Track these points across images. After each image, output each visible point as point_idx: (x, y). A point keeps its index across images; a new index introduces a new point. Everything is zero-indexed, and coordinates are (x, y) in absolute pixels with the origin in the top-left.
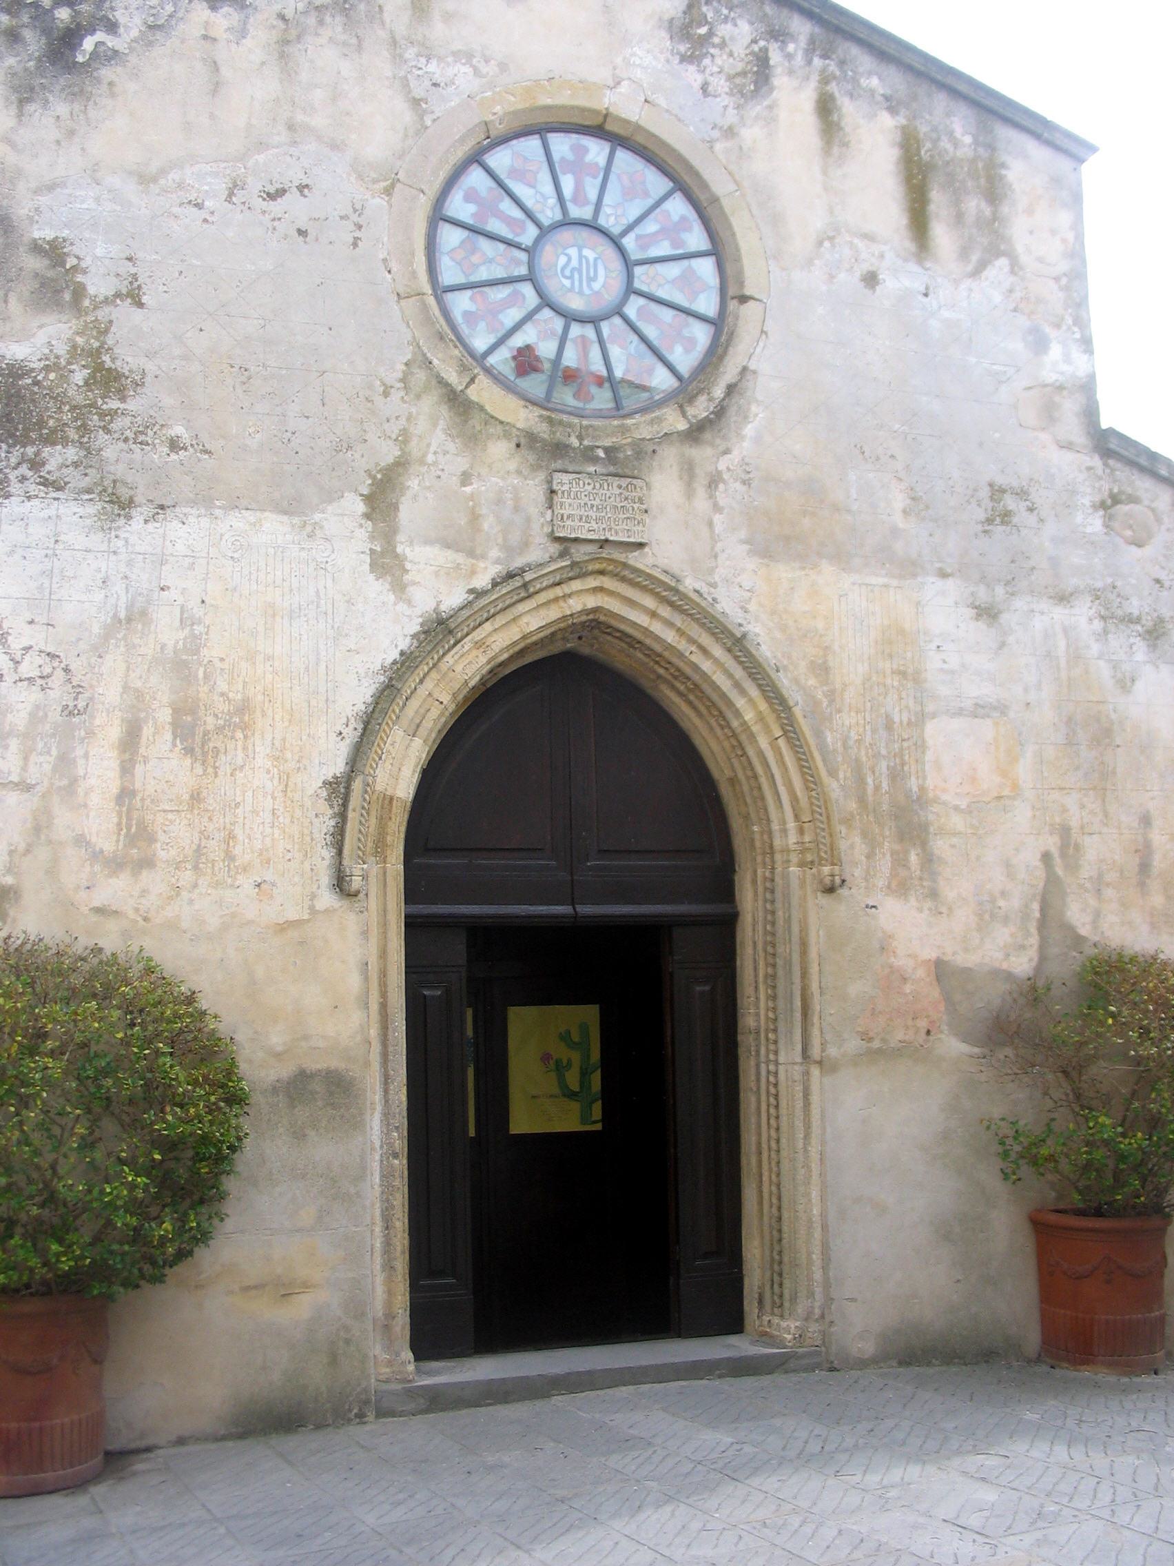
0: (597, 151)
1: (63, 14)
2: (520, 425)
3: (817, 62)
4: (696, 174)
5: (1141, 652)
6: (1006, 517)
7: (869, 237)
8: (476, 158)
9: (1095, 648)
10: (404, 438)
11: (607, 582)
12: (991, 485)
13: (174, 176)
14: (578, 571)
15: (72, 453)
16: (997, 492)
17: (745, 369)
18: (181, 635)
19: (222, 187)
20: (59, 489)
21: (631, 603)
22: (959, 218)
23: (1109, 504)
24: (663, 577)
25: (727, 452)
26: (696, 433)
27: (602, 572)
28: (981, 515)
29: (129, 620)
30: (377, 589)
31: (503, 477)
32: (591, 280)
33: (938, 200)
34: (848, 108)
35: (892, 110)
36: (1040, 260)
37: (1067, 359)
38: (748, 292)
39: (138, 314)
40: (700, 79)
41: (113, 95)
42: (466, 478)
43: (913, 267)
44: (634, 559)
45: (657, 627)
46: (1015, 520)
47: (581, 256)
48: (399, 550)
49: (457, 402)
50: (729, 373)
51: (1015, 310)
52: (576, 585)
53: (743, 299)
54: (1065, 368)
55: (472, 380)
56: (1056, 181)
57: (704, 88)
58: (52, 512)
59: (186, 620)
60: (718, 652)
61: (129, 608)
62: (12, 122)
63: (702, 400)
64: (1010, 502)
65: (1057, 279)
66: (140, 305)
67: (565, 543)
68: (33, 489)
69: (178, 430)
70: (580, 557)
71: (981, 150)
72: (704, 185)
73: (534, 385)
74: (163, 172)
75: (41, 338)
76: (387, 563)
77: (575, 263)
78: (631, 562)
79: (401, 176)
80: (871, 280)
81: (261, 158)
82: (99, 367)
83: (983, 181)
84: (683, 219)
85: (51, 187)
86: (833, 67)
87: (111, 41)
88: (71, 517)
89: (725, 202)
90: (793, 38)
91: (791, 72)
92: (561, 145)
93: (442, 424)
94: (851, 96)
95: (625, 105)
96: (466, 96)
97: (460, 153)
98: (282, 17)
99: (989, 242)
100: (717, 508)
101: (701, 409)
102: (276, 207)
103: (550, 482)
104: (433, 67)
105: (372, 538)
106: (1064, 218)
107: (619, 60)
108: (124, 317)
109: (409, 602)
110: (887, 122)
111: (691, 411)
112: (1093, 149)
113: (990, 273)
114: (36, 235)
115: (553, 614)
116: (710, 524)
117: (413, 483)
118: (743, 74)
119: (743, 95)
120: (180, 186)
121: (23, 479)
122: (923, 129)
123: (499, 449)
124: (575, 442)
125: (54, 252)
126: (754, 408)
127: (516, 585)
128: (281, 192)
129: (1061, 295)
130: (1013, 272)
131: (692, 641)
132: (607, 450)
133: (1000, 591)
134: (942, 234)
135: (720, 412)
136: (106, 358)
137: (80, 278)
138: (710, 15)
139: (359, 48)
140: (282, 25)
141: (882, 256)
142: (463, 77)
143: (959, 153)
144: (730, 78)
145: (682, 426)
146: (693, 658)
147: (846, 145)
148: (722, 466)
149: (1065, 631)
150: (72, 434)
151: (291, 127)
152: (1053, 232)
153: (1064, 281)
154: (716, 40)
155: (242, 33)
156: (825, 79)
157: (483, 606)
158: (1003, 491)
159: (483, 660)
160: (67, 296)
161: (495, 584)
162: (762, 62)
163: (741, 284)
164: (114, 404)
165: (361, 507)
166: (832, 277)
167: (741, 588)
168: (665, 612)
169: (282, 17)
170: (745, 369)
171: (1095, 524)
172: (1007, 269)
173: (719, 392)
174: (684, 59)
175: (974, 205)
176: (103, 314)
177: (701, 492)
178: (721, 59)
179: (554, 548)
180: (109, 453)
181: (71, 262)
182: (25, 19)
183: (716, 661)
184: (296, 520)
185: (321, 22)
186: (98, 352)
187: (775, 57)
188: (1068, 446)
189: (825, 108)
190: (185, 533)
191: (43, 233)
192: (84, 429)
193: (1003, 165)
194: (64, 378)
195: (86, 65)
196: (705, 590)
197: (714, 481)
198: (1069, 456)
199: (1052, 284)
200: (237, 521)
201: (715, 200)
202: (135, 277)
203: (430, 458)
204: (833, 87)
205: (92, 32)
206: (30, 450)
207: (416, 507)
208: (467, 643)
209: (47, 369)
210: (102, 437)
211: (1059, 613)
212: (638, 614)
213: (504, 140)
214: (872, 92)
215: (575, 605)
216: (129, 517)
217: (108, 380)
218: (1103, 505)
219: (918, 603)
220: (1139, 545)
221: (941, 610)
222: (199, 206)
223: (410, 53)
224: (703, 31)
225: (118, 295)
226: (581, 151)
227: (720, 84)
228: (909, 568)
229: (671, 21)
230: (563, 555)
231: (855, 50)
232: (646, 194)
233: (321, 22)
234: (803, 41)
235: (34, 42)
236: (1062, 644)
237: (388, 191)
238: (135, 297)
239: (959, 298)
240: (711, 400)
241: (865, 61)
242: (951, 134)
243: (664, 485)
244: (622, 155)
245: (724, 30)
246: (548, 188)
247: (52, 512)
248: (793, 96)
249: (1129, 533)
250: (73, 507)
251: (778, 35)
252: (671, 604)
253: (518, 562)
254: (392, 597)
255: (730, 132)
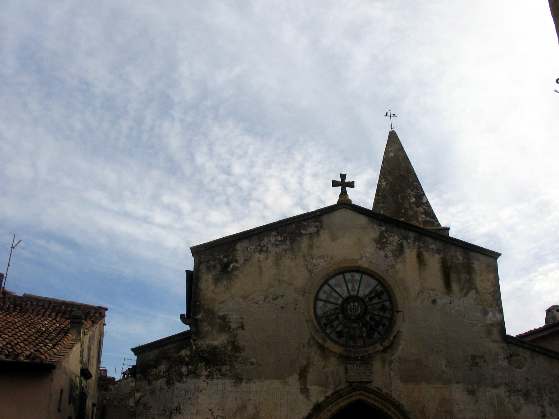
0: (357, 276)
1: (225, 260)
2: (338, 352)
3: (417, 243)
4: (384, 279)
5: (522, 401)
6: (477, 364)
7: (433, 290)
8: (326, 282)
9: (507, 400)
10: (308, 358)
11: (362, 392)
12: (472, 356)
13: (251, 297)
14: (354, 390)
15: (228, 367)
16: (474, 357)
17: (399, 331)
18: (254, 411)
19: (263, 298)
20: (225, 376)
21: (369, 397)
22: (459, 280)
23: (509, 358)
24: (377, 391)
25: (394, 354)
26: (385, 350)
27: (360, 390)
28: (469, 364)
29: (241, 408)
30: (302, 397)
31: (334, 366)
32: (356, 311)
33: (453, 276)
34: (426, 254)
35: (439, 254)
36: (485, 289)
37: (494, 316)
38: (399, 310)
39: (243, 332)
40: (384, 253)
41: (237, 278)
42: (324, 367)
43: (447, 296)
44: (368, 386)
45: (376, 403)
46: (480, 365)
47: (354, 305)
48: (308, 387)
49: (322, 348)
50: (394, 333)
51: (478, 304)
52: (354, 393)
53: (398, 312)
54: (494, 319)
55: (325, 342)
56: (489, 265)
57: (386, 256)
58: (223, 382)
59: (255, 407)
60: (392, 409)
61: (242, 405)
62: (214, 287)
63: (387, 341)
64: (478, 360)
65: (490, 294)
66: (244, 329)
67: (351, 383)
68: (219, 376)
69: (253, 360)
70: (353, 386)
71: (466, 260)
72: (386, 282)
73: (342, 340)
74: (249, 296)
75: (221, 339)
76: (304, 391)
77: (352, 307)
78: (368, 387)
79: (307, 290)
80: (434, 302)
81: (272, 289)
82: (234, 346)
83: (466, 269)
84: (381, 291)
85: (223, 302)
86: (421, 244)
87: (236, 265)
88: (228, 383)
89: (392, 286)
90: (410, 238)
91: (409, 248)
92: (348, 276)
93: (318, 354)
94: (427, 251)
95: (364, 264)
96: (322, 265)
97: (322, 282)
98: (276, 253)
99: (469, 285)
100: (391, 370)
101: (386, 343)
102: (276, 302)
103: (346, 367)
104: (314, 261)
105: (301, 384)
106: (492, 276)
107: (362, 252)
108: (241, 333)
109: (310, 401)
110: (437, 256)
111: (384, 344)
112: (499, 255)
113: (470, 294)
114: (220, 314)
115: (348, 401)
116: (390, 374)
117: (311, 370)
118: (396, 250)
119: (396, 256)
120: (253, 299)
121: (217, 374)
122: (448, 257)
123: (333, 359)
124: (353, 355)
125: (224, 318)
126: (401, 341)
127: (338, 395)
128: (277, 298)
129: (492, 298)
130: (476, 293)
131: (385, 406)
132: (361, 357)
133: (475, 386)
134: (455, 287)
135: (392, 343)
136: (236, 343)
137: (229, 324)
138: (386, 236)
139: (296, 259)
140: (276, 255)
141: (437, 294)
142: (322, 262)
143: (459, 262)
144: (392, 252)
145: (381, 348)
146: (386, 411)
147: (426, 265)
148: (393, 358)
149: (496, 396)
150: (228, 363)
151: (279, 281)
152: (488, 280)
153: (492, 294)
154: (388, 242)
155: (267, 259)
156: (419, 248)
157: (328, 401)
158: (475, 357)
159: (329, 415)
160: (227, 329)
161: (332, 394)
162: (401, 246)
163: (397, 307)
164: (238, 354)
165: (298, 377)
166: (422, 302)
167: (399, 391)
168: (378, 399)
169: (276, 253)
170: (399, 331)
171: (505, 364)
172: (475, 293)
173: (391, 338)
174: (380, 249)
175: (464, 276)
176: (235, 332)
177: (387, 366)
178: (390, 247)
179: (348, 384)
180: (237, 367)
181: (227, 320)
182: (217, 262)
183: (393, 412)
184: (282, 381)
185: (286, 253)
186: (234, 342)
187: (405, 244)
188: (496, 342)
189: (420, 256)
190: (254, 386)
191: (221, 314)
192: (231, 361)
193: (473, 263)
194: (226, 349)
195: (231, 271)
196: (388, 392)
197: (391, 362)
198: (496, 345)
199: (489, 295)
200: (268, 382)
201: (389, 286)
202: (242, 322)
203: (315, 363)
204: (422, 250)
205: (232, 263)
206: (218, 367)
207: (311, 376)
208: (325, 411)
209: (222, 347)
210: (235, 363)
211: (494, 391)
212: (371, 400)
213: (333, 277)
214: (432, 249)
215: (354, 399)
216: (241, 383)
217: (237, 349)
218: (507, 358)
219: (451, 392)
220: (520, 368)
221: (458, 393)
222: (258, 303)
223: (308, 258)
224: (385, 240)
225: (238, 327)
226: (353, 277)
227: (390, 254)
228: (447, 382)
229: (376, 239)
230: (350, 386)
231: (427, 238)
232: (371, 286)
233: (286, 253)
234: (412, 238)
235: (219, 267)
236: (496, 400)
237: (303, 295)
238: (242, 327)
239: (462, 303)
240: (389, 340)
241: (430, 241)
242: (456, 257)
243: (377, 365)
244: (364, 277)
245: (391, 239)
246: (345, 288)
247: (223, 382)
248: (410, 254)
249: (516, 365)
250: (228, 381)
251: (406, 238)
252: (379, 397)
253: (338, 389)
254: (306, 400)
255: (393, 267)
